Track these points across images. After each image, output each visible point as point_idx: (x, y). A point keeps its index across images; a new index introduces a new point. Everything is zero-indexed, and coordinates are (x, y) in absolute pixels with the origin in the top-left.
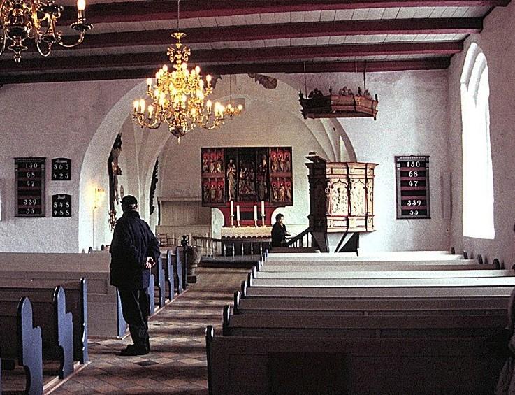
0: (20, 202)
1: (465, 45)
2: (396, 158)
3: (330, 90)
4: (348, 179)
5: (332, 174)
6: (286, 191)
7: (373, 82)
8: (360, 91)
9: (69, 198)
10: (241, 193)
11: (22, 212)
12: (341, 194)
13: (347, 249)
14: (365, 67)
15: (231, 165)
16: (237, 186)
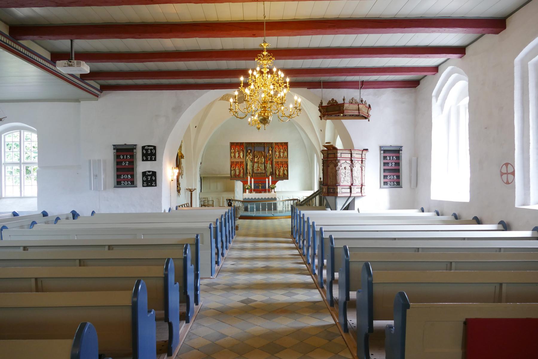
0: (118, 176)
1: (440, 68)
2: (381, 147)
3: (344, 100)
4: (352, 161)
5: (341, 157)
6: (284, 170)
7: (367, 95)
8: (362, 101)
9: (154, 174)
10: (255, 171)
11: (119, 184)
12: (347, 171)
13: (347, 208)
14: (364, 85)
15: (249, 154)
16: (253, 167)
